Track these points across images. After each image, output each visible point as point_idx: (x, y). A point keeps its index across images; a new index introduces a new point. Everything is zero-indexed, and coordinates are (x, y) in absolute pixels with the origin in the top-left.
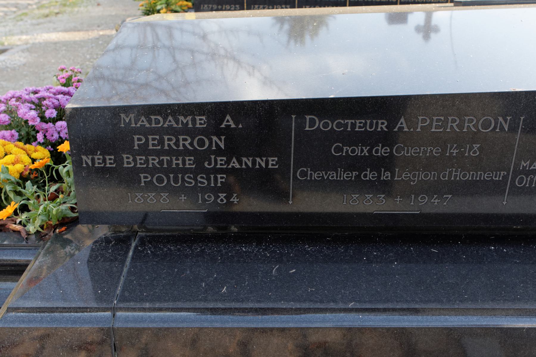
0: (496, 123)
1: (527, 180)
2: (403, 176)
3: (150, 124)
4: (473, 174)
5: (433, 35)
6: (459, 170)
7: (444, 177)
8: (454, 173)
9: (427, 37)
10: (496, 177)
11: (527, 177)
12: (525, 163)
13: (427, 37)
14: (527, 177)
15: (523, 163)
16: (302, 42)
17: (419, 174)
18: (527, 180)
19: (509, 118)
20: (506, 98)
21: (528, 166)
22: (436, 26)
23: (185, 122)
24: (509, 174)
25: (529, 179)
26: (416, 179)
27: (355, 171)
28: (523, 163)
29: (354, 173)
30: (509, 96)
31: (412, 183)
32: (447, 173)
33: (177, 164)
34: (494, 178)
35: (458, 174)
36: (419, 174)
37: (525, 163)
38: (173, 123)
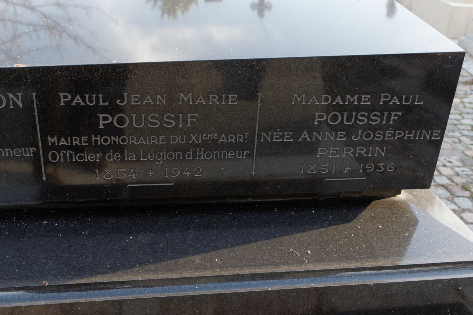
0: (8, 100)
1: (60, 156)
2: (149, 157)
3: (320, 102)
4: (217, 153)
5: (266, 12)
6: (202, 149)
7: (189, 157)
8: (198, 153)
9: (261, 14)
10: (26, 154)
11: (59, 153)
12: (52, 138)
13: (261, 14)
14: (59, 153)
15: (50, 139)
16: (174, 12)
17: (163, 154)
18: (60, 156)
19: (165, 96)
20: (10, 74)
21: (56, 142)
22: (269, 3)
23: (352, 100)
24: (39, 150)
25: (62, 155)
26: (161, 159)
27: (98, 153)
28: (50, 139)
29: (98, 155)
30: (11, 72)
31: (157, 163)
32: (191, 153)
33: (200, 151)
34: (24, 154)
35: (202, 153)
36: (163, 154)
37: (52, 138)
38: (80, 101)
